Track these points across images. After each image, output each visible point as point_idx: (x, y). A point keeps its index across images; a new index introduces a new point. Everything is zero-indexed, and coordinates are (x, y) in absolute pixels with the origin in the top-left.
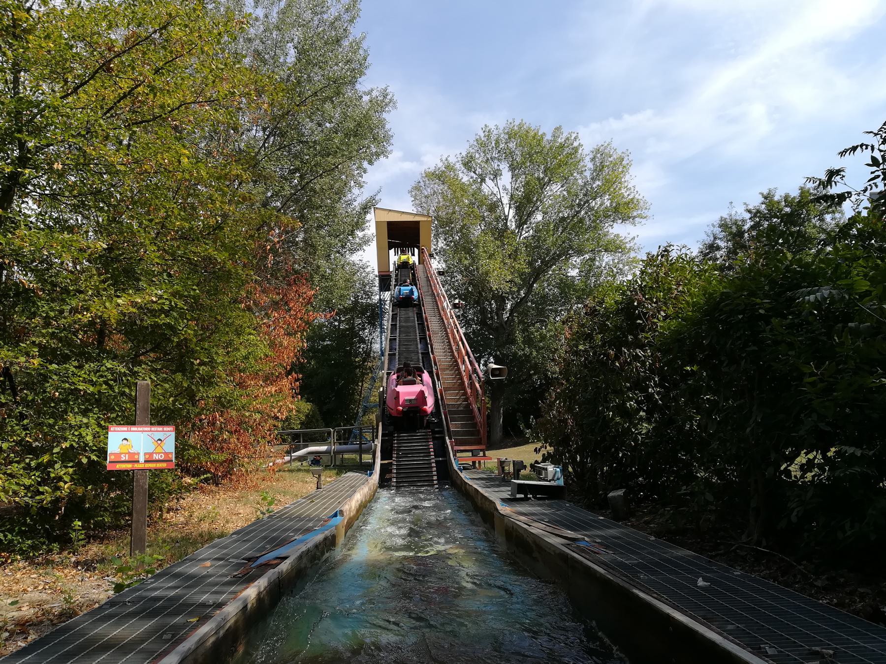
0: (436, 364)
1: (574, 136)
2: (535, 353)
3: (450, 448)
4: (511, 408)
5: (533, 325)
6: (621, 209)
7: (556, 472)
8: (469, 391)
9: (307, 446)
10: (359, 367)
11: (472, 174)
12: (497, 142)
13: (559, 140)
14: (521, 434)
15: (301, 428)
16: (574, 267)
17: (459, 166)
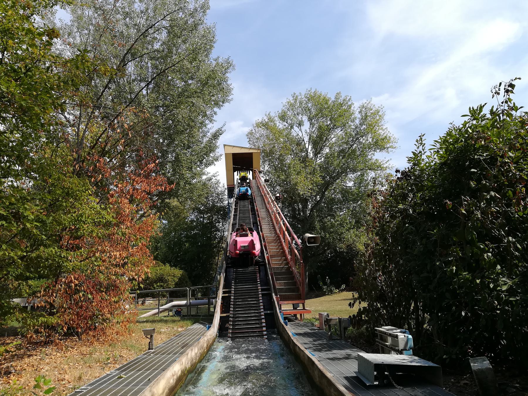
1: (348, 98)
2: (328, 236)
3: (276, 303)
4: (326, 269)
5: (326, 217)
6: (380, 142)
7: (408, 339)
8: (289, 257)
9: (172, 301)
10: (215, 247)
11: (285, 123)
12: (301, 103)
14: (320, 289)
15: (175, 287)
16: (350, 180)
17: (276, 119)
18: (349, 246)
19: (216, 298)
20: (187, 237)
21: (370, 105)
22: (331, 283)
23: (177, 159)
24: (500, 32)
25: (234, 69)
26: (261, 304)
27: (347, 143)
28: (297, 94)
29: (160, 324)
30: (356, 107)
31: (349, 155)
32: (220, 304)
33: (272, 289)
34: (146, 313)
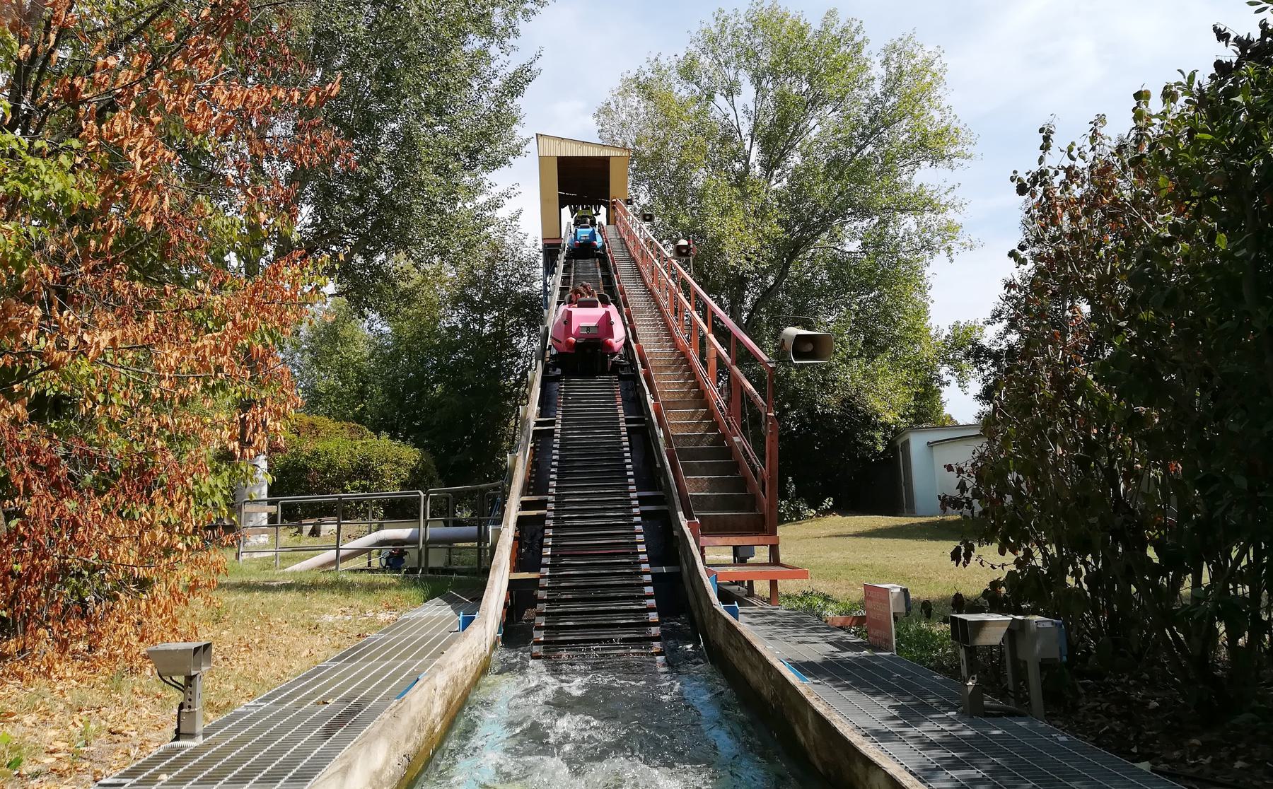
1: (856, 24)
2: (794, 373)
6: (931, 142)
11: (695, 87)
13: (833, 32)
16: (853, 236)
18: (844, 400)
19: (498, 522)
20: (441, 369)
21: (910, 45)
22: (799, 494)
23: (407, 141)
28: (729, 11)
29: (327, 596)
31: (854, 170)
32: (510, 540)
33: (676, 497)
34: (303, 559)
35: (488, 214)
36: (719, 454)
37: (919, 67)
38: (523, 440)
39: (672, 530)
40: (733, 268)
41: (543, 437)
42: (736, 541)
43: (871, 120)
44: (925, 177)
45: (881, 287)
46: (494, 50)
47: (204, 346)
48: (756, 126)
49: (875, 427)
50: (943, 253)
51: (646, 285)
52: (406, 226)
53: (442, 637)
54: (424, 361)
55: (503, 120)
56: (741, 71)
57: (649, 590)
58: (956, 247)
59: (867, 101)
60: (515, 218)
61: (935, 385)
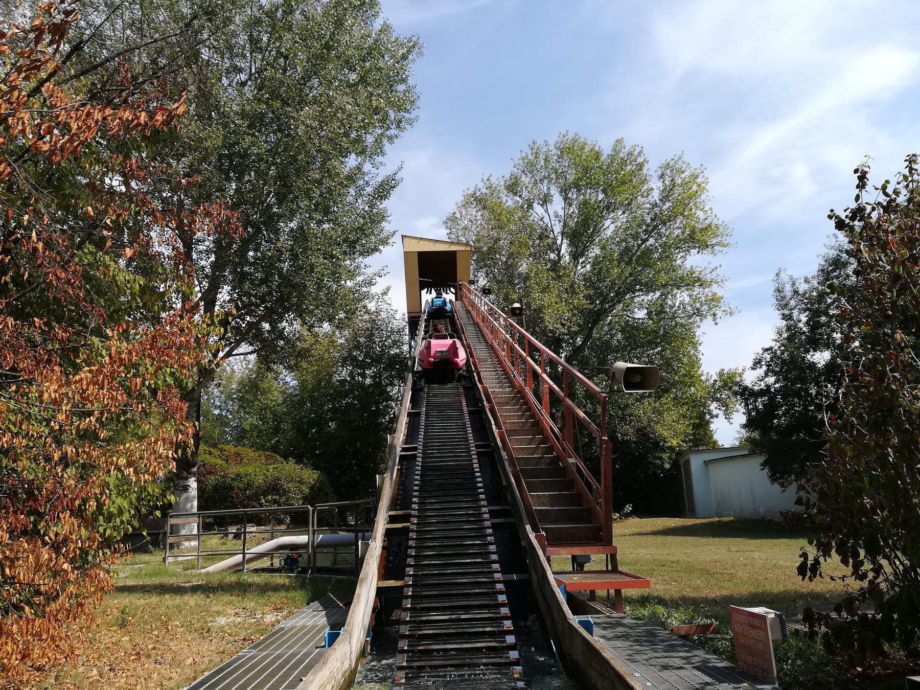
0: (489, 400)
6: (698, 236)
11: (518, 198)
13: (621, 155)
16: (641, 306)
21: (680, 163)
23: (300, 235)
24: (882, 68)
25: (421, 54)
26: (494, 557)
27: (636, 237)
28: (540, 142)
29: (226, 598)
30: (652, 169)
31: (639, 257)
33: (523, 512)
35: (364, 289)
36: (554, 473)
37: (687, 180)
38: (390, 463)
39: (519, 541)
40: (551, 331)
41: (407, 460)
42: (578, 551)
43: (652, 219)
44: (693, 261)
45: (668, 339)
46: (367, 167)
47: (81, 379)
48: (565, 226)
49: (663, 450)
50: (710, 318)
51: (486, 342)
52: (301, 297)
53: (307, 655)
54: (322, 405)
55: (375, 219)
56: (552, 187)
57: (502, 598)
58: (719, 313)
59: (648, 206)
60: (385, 293)
61: (708, 417)
